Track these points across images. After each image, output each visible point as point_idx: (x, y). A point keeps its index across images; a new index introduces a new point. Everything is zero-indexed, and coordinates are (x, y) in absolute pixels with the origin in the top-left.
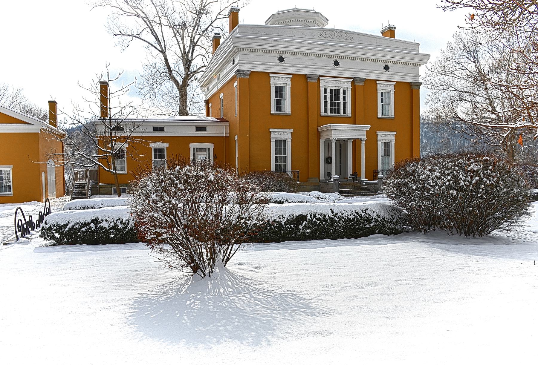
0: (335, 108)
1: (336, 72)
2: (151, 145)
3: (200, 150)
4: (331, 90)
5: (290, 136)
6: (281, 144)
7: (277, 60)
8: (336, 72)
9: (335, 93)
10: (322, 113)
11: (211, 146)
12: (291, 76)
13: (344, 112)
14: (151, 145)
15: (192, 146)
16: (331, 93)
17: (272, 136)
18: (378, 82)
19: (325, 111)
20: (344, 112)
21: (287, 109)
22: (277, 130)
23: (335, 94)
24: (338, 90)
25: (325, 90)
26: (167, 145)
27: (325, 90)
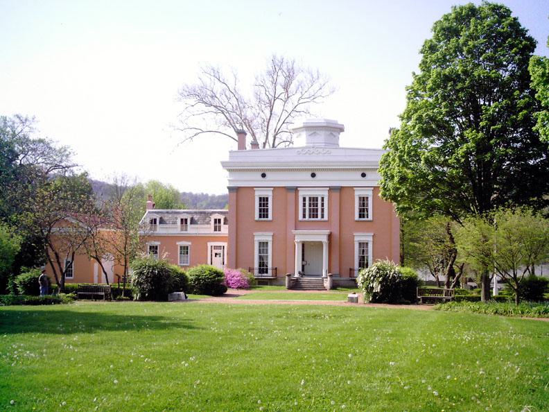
0: (264, 213)
1: (313, 183)
2: (178, 243)
3: (216, 247)
4: (310, 198)
5: (370, 239)
6: (263, 245)
7: (360, 177)
8: (313, 183)
9: (314, 200)
10: (301, 218)
11: (225, 244)
12: (372, 188)
13: (323, 217)
14: (178, 243)
15: (209, 244)
16: (310, 200)
17: (256, 239)
18: (355, 189)
19: (304, 216)
20: (323, 217)
21: (326, 218)
22: (260, 233)
23: (264, 201)
24: (317, 198)
25: (304, 199)
26: (190, 243)
27: (304, 199)
